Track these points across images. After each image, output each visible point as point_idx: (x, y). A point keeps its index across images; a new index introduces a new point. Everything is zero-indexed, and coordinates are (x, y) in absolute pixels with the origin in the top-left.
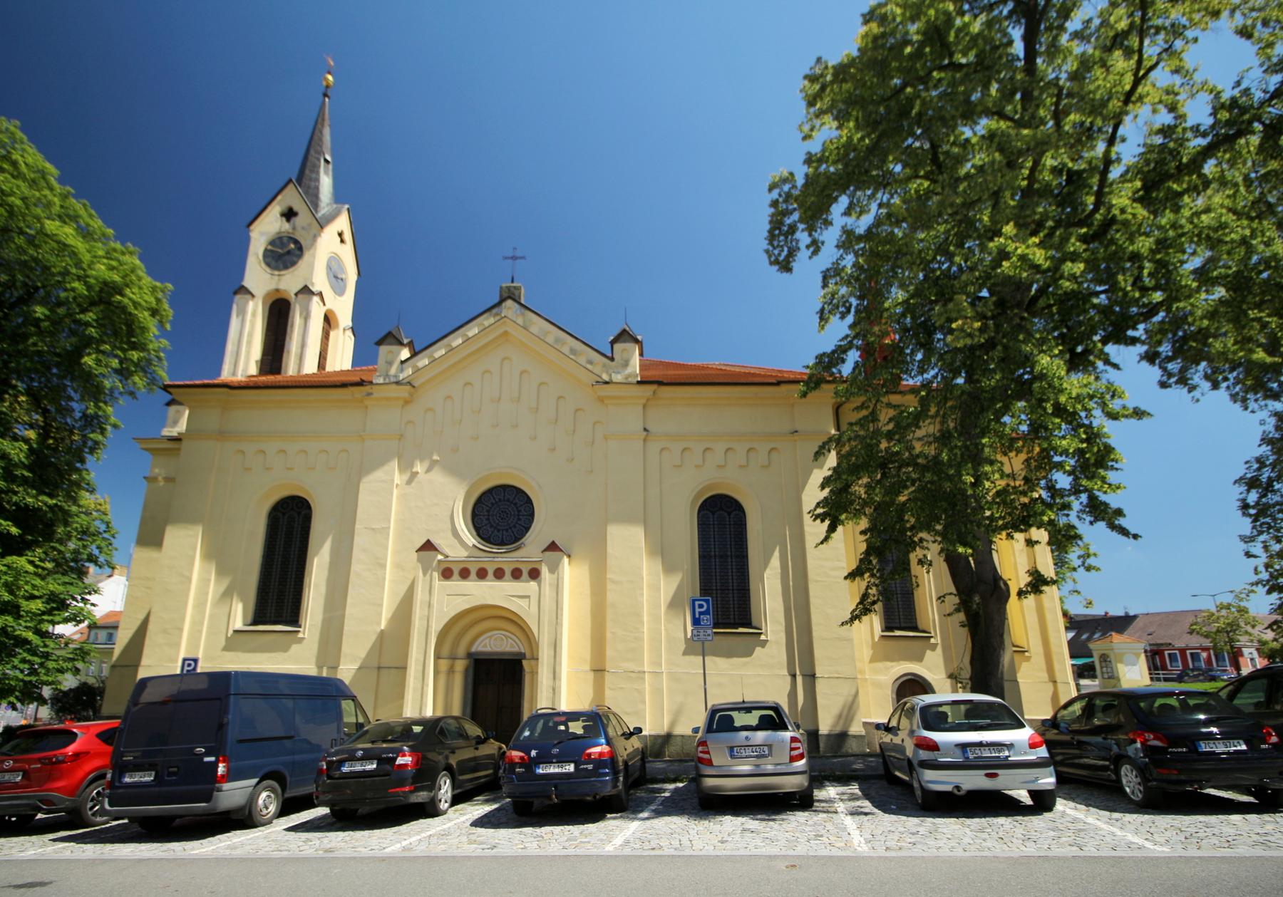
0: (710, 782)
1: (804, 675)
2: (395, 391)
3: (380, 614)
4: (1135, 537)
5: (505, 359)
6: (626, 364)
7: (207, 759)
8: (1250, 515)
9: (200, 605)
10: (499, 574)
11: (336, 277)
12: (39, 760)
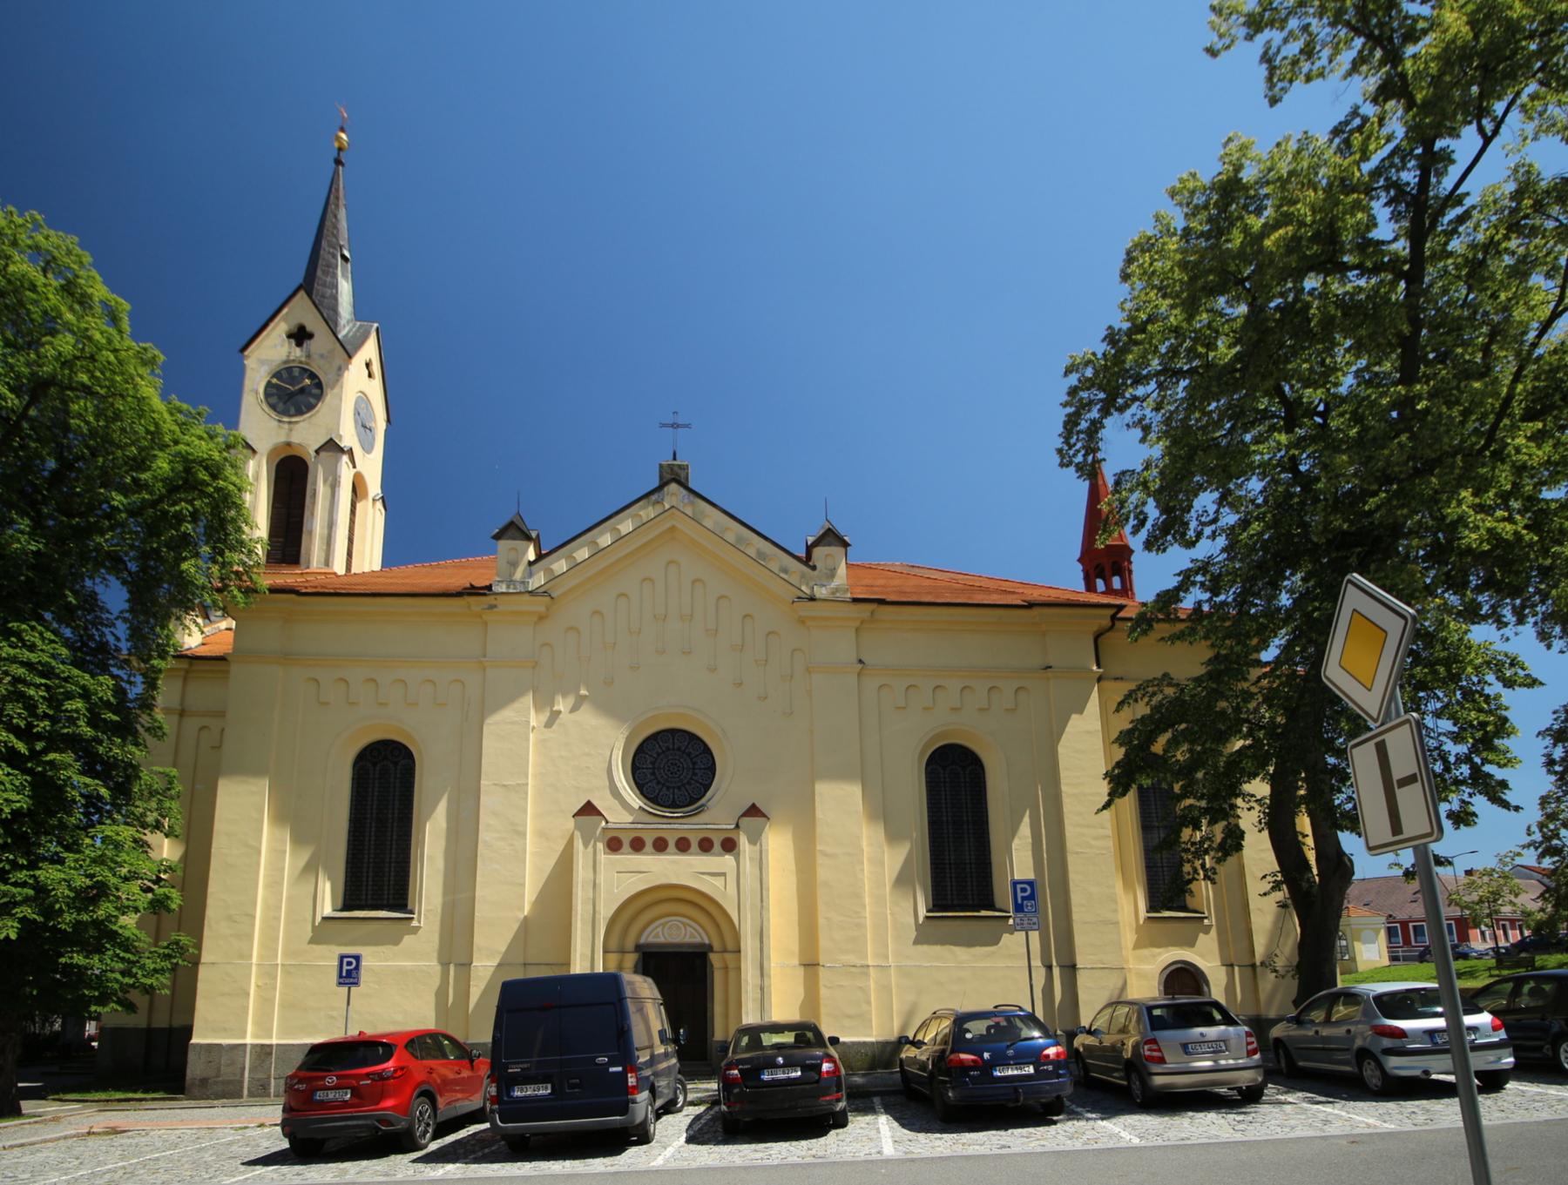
0: (1159, 1080)
1: (1061, 966)
2: (527, 604)
3: (523, 895)
4: (1517, 809)
5: (670, 563)
6: (832, 574)
7: (612, 1069)
8: (1556, 773)
9: (274, 884)
10: (683, 846)
11: (364, 426)
12: (367, 1076)
